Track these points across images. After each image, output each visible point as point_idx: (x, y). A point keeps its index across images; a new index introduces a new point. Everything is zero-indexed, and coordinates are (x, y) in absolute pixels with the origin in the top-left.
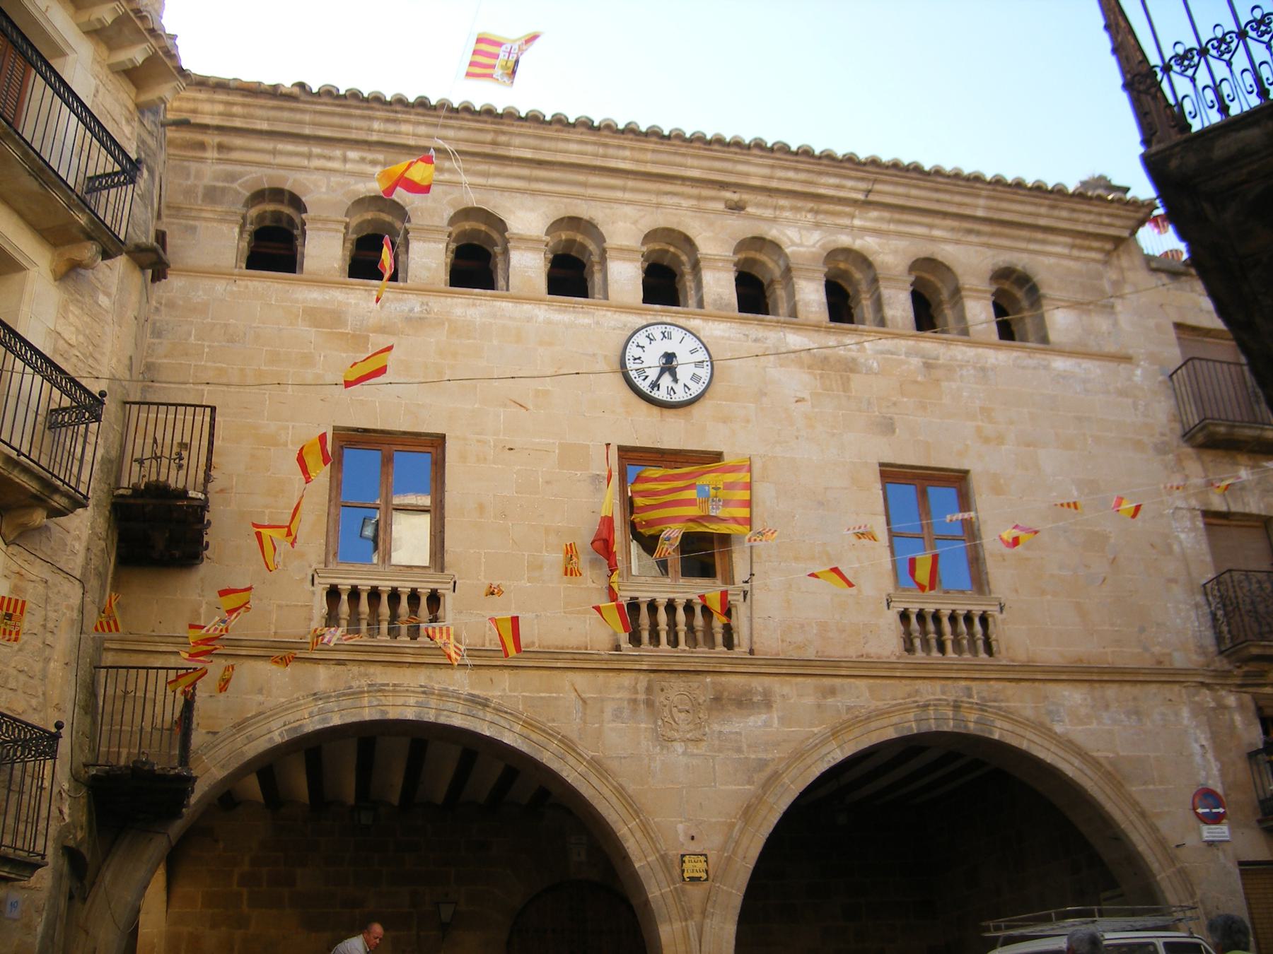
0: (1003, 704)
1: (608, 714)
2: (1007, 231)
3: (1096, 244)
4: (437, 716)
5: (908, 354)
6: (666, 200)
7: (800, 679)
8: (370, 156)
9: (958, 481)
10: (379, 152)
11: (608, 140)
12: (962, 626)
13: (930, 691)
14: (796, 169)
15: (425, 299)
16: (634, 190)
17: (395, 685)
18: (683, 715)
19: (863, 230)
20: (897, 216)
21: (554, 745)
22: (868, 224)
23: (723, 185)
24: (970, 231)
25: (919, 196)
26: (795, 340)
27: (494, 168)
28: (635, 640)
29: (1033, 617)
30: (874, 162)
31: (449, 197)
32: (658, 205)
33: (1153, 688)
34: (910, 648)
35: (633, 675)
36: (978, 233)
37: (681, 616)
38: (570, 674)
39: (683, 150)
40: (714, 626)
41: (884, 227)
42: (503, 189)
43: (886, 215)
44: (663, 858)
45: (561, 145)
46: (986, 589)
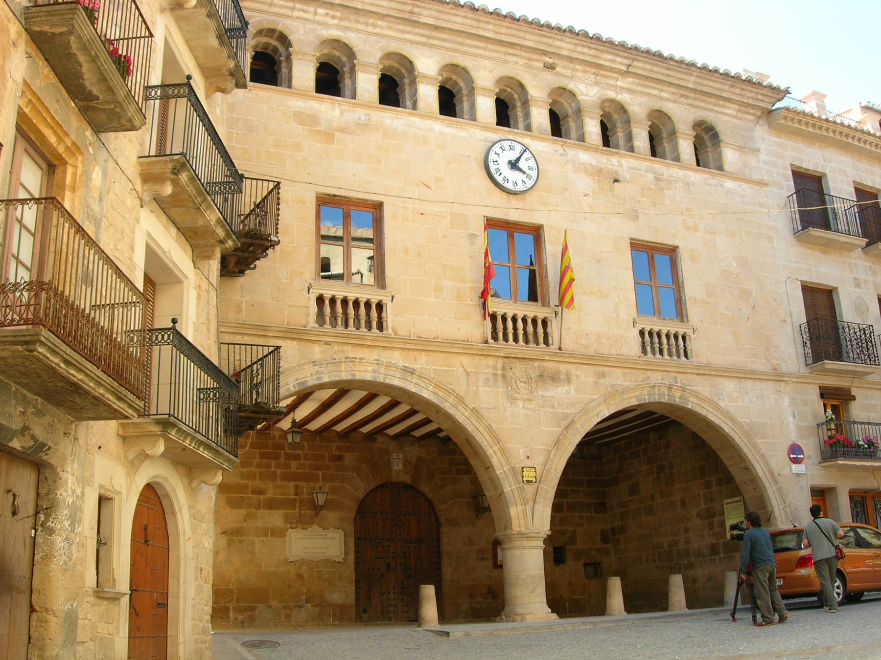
0: (693, 388)
1: (481, 382)
2: (703, 98)
3: (751, 111)
4: (385, 379)
5: (646, 171)
6: (509, 58)
7: (586, 367)
8: (332, 13)
9: (672, 252)
10: (337, 11)
11: (481, 18)
12: (673, 340)
13: (656, 378)
14: (589, 48)
15: (368, 112)
16: (490, 50)
17: (360, 358)
18: (522, 385)
19: (622, 88)
20: (643, 82)
21: (452, 399)
22: (626, 85)
23: (544, 53)
24: (683, 96)
25: (658, 71)
26: (584, 157)
27: (408, 28)
28: (495, 337)
29: (713, 334)
30: (636, 48)
31: (379, 45)
32: (505, 61)
33: (771, 384)
34: (644, 351)
35: (495, 359)
36: (687, 97)
37: (520, 325)
38: (460, 356)
39: (525, 29)
40: (538, 331)
41: (634, 87)
42: (412, 42)
43: (637, 81)
44: (513, 468)
45: (452, 18)
46: (685, 319)
